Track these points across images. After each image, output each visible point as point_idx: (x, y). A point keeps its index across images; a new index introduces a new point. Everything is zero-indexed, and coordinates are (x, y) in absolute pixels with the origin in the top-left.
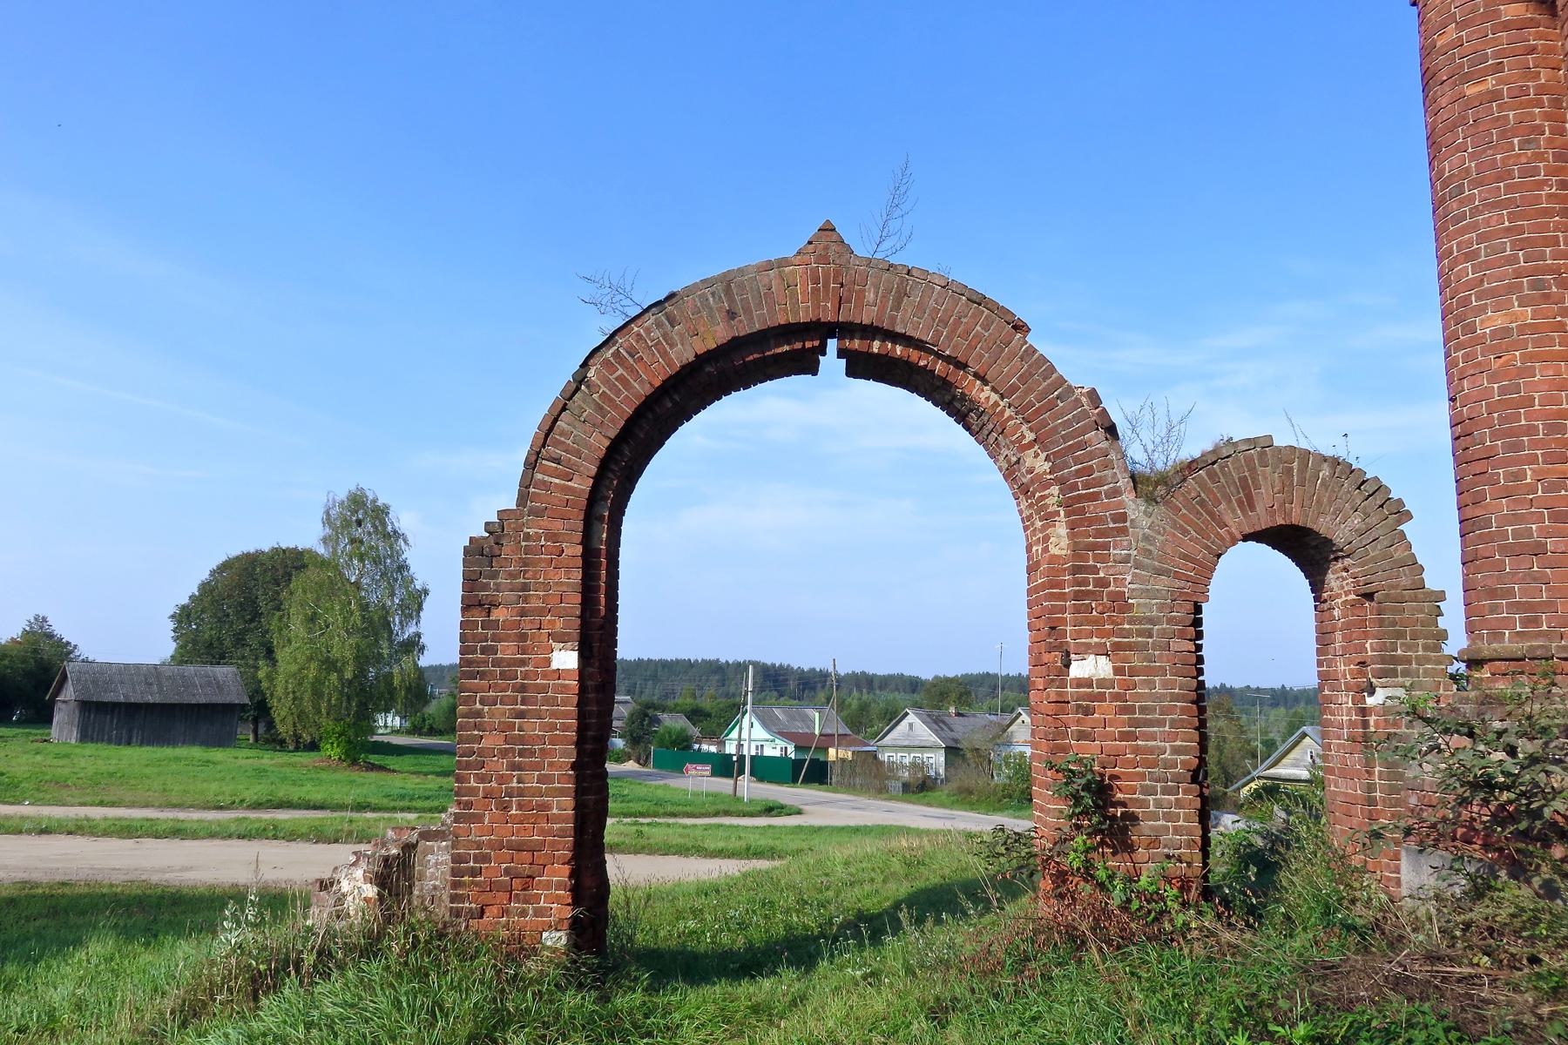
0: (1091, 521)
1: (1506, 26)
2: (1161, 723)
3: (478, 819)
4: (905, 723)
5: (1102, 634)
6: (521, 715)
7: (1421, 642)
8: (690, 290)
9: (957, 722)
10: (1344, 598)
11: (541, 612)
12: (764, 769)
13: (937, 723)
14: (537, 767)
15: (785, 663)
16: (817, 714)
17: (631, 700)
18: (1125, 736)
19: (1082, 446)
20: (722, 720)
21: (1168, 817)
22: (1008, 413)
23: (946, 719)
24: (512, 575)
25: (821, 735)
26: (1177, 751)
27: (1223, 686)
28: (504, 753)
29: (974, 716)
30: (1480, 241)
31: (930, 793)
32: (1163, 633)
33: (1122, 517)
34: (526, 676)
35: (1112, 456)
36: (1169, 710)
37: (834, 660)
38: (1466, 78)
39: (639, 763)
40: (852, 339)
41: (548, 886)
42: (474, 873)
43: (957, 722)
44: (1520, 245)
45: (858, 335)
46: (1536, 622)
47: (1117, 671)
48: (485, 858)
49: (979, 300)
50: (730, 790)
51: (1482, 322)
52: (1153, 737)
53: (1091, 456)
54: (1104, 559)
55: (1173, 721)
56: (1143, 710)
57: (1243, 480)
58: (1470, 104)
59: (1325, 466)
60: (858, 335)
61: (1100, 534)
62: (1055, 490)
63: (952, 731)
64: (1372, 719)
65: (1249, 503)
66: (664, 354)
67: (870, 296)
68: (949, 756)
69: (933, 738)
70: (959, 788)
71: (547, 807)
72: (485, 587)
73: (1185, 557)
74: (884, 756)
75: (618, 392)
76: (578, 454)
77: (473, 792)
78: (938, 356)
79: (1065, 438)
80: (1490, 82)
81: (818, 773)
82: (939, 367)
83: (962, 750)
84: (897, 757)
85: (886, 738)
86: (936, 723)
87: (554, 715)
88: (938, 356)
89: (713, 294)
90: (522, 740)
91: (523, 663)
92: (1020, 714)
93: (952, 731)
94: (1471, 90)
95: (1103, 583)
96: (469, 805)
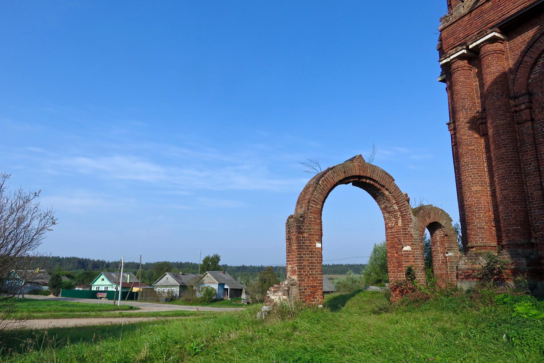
0: (406, 219)
1: (475, 138)
2: (419, 259)
3: (304, 280)
4: (165, 278)
5: (410, 242)
6: (311, 257)
7: (455, 244)
8: (337, 166)
9: (182, 277)
10: (440, 236)
11: (314, 235)
12: (111, 295)
13: (176, 277)
14: (315, 269)
15: (88, 258)
16: (129, 275)
17: (45, 271)
18: (414, 262)
19: (404, 204)
20: (80, 279)
21: (421, 277)
22: (391, 197)
23: (179, 276)
24: (308, 226)
25: (129, 283)
26: (422, 264)
27: (243, 266)
28: (308, 266)
29: (187, 275)
30: (472, 174)
31: (175, 302)
32: (418, 242)
33: (411, 219)
34: (311, 249)
35: (409, 207)
36: (420, 257)
37: (141, 255)
38: (469, 145)
39: (54, 295)
40: (364, 179)
41: (318, 295)
42: (304, 292)
43: (182, 277)
44: (479, 176)
45: (365, 178)
46: (484, 240)
47: (412, 249)
48: (305, 289)
49: (386, 174)
50: (113, 304)
51: (473, 188)
52: (417, 262)
53: (406, 207)
54: (408, 227)
55: (421, 258)
56: (416, 256)
57: (429, 213)
58: (470, 150)
59: (440, 211)
60: (365, 178)
61: (408, 222)
62: (399, 213)
63: (181, 280)
64: (447, 258)
65: (430, 217)
66: (333, 179)
67: (369, 171)
68: (181, 289)
69: (176, 282)
70: (186, 299)
71: (317, 277)
72: (302, 229)
73: (421, 227)
74: (157, 289)
75: (325, 187)
76: (318, 200)
77: (303, 274)
78: (379, 184)
79: (402, 203)
80: (473, 147)
81: (133, 296)
82: (379, 186)
83: (187, 286)
84: (161, 289)
85: (158, 283)
86: (176, 277)
87: (317, 257)
88: (379, 184)
89: (341, 167)
90: (311, 263)
91: (311, 246)
92: (207, 273)
93: (181, 280)
94: (470, 148)
95: (409, 232)
96: (302, 278)
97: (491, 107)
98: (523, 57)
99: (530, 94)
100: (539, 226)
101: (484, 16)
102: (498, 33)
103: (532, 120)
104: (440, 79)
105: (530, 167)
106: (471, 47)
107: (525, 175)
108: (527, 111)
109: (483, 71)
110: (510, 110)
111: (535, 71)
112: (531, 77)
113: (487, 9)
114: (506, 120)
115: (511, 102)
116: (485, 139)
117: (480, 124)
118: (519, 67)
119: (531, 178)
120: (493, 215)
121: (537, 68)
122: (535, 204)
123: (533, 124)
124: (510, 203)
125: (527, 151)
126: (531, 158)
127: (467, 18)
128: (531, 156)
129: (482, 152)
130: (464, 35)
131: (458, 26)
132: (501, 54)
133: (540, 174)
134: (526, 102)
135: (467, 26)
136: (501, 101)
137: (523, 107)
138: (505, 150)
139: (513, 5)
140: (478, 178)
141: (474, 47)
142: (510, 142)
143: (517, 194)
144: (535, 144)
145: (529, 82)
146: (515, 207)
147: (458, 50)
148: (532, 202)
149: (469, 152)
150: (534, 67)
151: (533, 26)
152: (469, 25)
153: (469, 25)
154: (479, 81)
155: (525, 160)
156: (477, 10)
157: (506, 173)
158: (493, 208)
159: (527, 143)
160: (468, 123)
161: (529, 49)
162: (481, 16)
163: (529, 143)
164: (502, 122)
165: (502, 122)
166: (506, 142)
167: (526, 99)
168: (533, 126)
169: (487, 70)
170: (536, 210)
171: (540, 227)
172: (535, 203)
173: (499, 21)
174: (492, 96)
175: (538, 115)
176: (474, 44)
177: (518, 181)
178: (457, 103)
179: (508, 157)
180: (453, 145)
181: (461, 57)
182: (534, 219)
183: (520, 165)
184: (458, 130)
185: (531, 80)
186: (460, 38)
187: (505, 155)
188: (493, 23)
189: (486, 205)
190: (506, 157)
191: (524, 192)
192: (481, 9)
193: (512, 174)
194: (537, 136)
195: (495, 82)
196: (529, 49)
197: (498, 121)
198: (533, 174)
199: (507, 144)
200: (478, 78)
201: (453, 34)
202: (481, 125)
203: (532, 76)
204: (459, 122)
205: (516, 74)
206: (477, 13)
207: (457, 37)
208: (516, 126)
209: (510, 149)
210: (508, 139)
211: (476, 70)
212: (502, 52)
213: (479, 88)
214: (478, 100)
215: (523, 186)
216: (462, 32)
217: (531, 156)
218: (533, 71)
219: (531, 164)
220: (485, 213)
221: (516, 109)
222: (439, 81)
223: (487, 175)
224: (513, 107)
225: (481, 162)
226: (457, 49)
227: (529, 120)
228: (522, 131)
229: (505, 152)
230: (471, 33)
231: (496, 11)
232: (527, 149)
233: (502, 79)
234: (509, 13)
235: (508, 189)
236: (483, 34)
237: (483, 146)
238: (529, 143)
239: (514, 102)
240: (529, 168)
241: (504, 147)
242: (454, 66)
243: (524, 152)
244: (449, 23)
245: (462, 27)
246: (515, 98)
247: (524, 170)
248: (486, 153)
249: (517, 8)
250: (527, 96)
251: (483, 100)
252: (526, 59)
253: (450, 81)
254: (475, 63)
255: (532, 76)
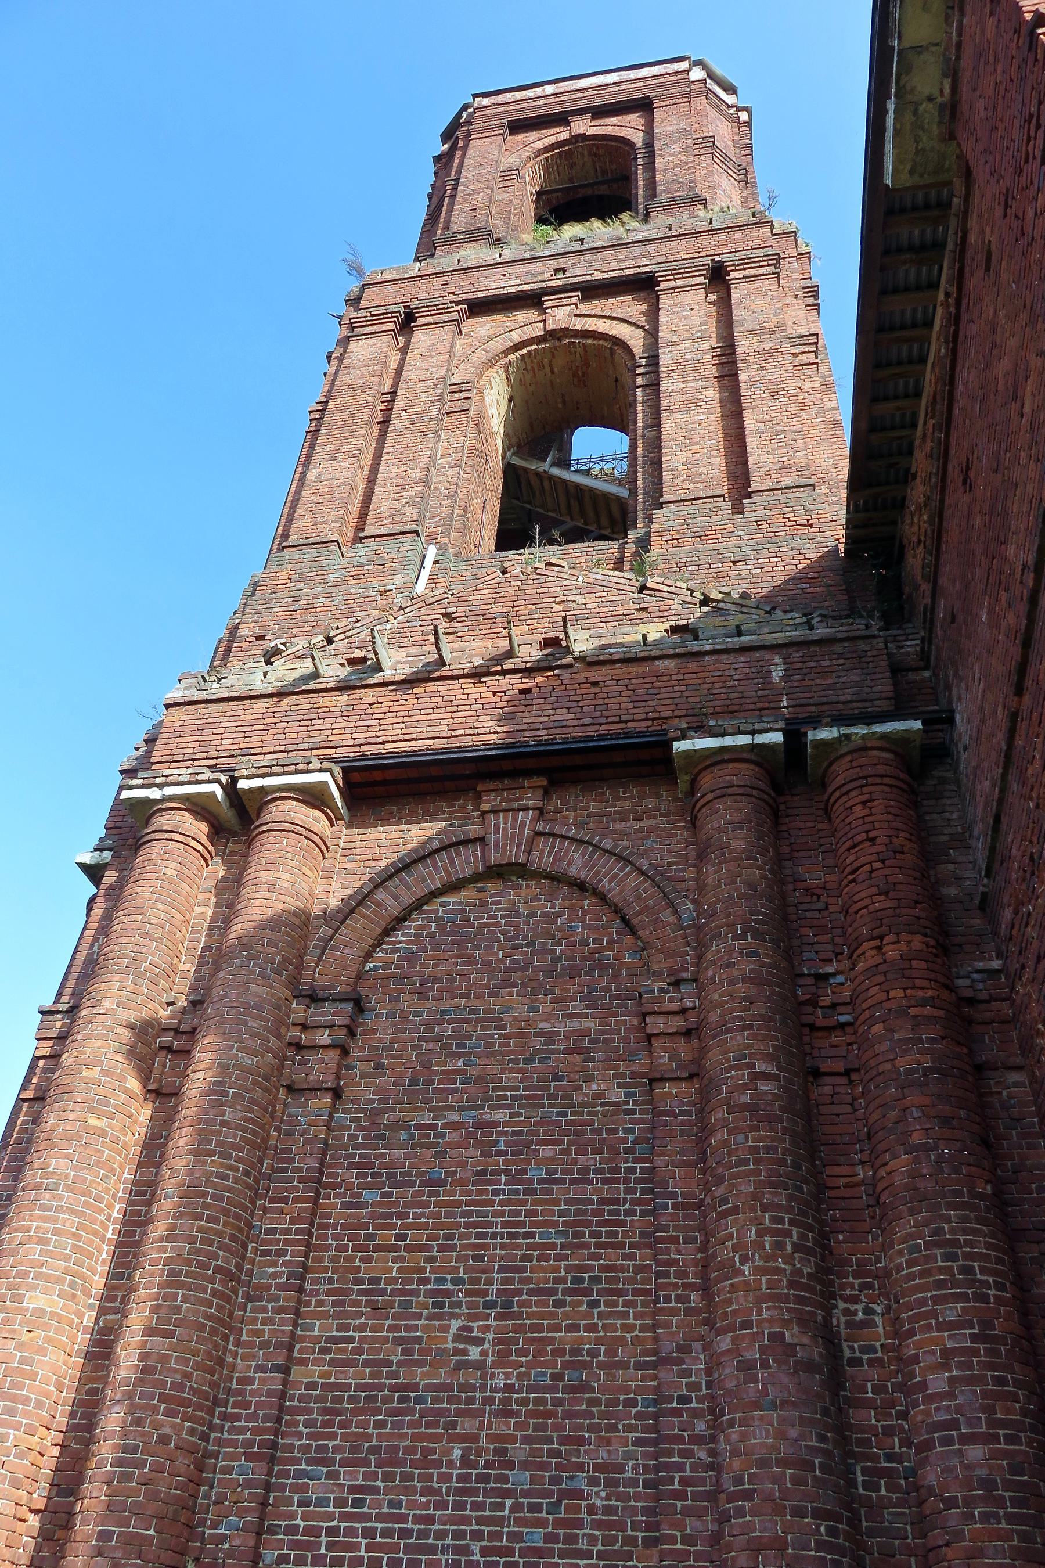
1: (126, 1091)
38: (92, 1110)
44: (77, 1250)
51: (31, 1297)
58: (88, 1129)
80: (103, 1123)
94: (92, 1121)
97: (232, 995)
98: (376, 887)
99: (359, 1005)
100: (223, 1538)
101: (314, 722)
102: (337, 785)
103: (337, 1093)
104: (87, 858)
105: (274, 1264)
106: (242, 784)
107: (248, 1293)
108: (333, 1056)
109: (249, 871)
110: (283, 1030)
111: (394, 943)
112: (375, 955)
113: (332, 709)
114: (262, 1058)
115: (294, 1005)
116: (155, 1111)
117: (161, 1048)
118: (352, 911)
119: (264, 1310)
120: (56, 1451)
121: (399, 935)
122: (242, 1430)
123: (334, 1109)
124: (155, 1402)
125: (285, 1200)
126: (287, 1232)
127: (261, 705)
128: (292, 1222)
129: (126, 1156)
130: (236, 746)
131: (228, 714)
132: (320, 848)
133: (299, 1302)
134: (339, 1026)
135: (254, 728)
136: (271, 987)
137: (325, 1037)
138: (221, 1165)
139: (403, 731)
140: (67, 1258)
141: (251, 790)
142: (247, 1141)
143: (197, 1366)
144: (319, 1182)
145: (367, 968)
146: (168, 1424)
147: (200, 777)
148: (237, 1417)
149: (81, 1137)
150: (394, 929)
151: (428, 816)
152: (261, 727)
153: (261, 727)
154: (217, 906)
155: (268, 1232)
156: (304, 700)
157: (188, 1262)
158: (72, 1415)
159: (296, 1170)
160: (131, 1027)
161: (399, 871)
162: (306, 717)
163: (300, 1170)
164: (248, 1061)
165: (248, 1061)
166: (235, 1136)
167: (340, 1014)
168: (331, 1116)
169: (262, 874)
170: (234, 1457)
171: (227, 1546)
172: (243, 1423)
173: (351, 752)
174: (249, 958)
175: (359, 1084)
176: (257, 783)
177: (220, 1308)
178: (120, 940)
179: (221, 1198)
180: (24, 1100)
181: (197, 806)
182: (216, 1503)
183: (245, 1246)
184: (80, 1037)
185: (371, 965)
186: (218, 748)
187: (214, 1186)
188: (333, 751)
189: (48, 1394)
190: (214, 1196)
191: (221, 1362)
192: (313, 700)
193: (210, 1272)
194: (332, 1157)
195: (274, 923)
196: (399, 871)
197: (234, 1051)
198: (277, 1299)
199: (234, 1146)
200: (216, 896)
201: (202, 729)
202: (164, 1053)
203: (380, 954)
204: (96, 1010)
205: (339, 928)
206: (299, 707)
207: (212, 743)
208: (282, 1092)
209: (237, 1170)
210: (245, 1130)
211: (222, 872)
212: (324, 847)
213: (209, 929)
214: (187, 967)
215: (226, 1338)
216: (235, 735)
217: (292, 1222)
218: (386, 939)
219: (280, 1253)
220: (30, 1432)
221: (301, 1038)
222: (79, 865)
223: (104, 1256)
224: (294, 1024)
225: (108, 1194)
226: (198, 774)
227: (327, 1089)
228: (294, 1120)
229: (219, 1176)
230: (259, 750)
231: (352, 724)
232: (286, 1190)
233: (297, 921)
234: (387, 746)
235: (171, 1334)
236: (296, 764)
237: (137, 1135)
238: (300, 1170)
239: (305, 1011)
240: (271, 1270)
241: (221, 1155)
242: (162, 821)
243: (272, 1200)
244: (204, 695)
245: (239, 724)
246: (313, 998)
247: (250, 1273)
248: (140, 1165)
249: (413, 743)
250: (348, 1007)
251: (205, 971)
252: (380, 895)
253: (120, 871)
254: (226, 847)
255: (380, 954)
